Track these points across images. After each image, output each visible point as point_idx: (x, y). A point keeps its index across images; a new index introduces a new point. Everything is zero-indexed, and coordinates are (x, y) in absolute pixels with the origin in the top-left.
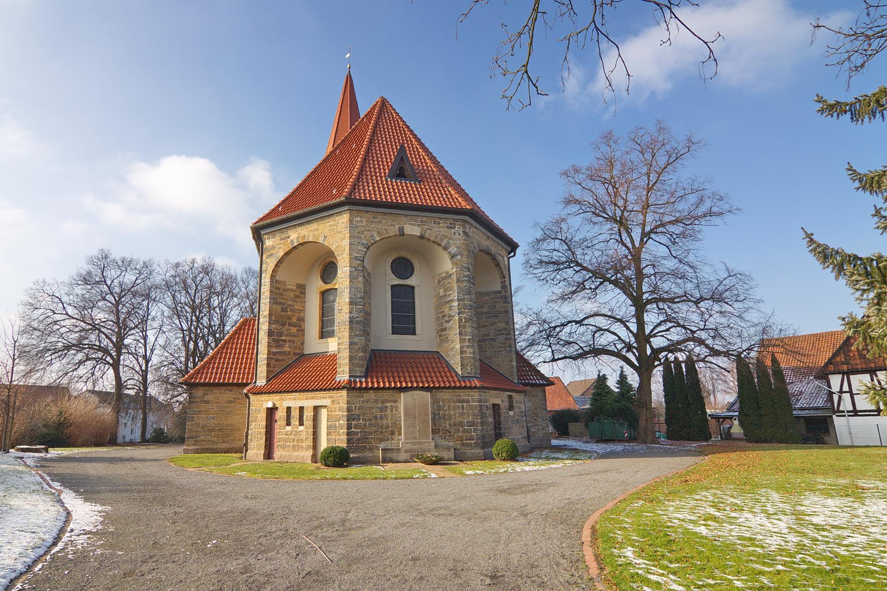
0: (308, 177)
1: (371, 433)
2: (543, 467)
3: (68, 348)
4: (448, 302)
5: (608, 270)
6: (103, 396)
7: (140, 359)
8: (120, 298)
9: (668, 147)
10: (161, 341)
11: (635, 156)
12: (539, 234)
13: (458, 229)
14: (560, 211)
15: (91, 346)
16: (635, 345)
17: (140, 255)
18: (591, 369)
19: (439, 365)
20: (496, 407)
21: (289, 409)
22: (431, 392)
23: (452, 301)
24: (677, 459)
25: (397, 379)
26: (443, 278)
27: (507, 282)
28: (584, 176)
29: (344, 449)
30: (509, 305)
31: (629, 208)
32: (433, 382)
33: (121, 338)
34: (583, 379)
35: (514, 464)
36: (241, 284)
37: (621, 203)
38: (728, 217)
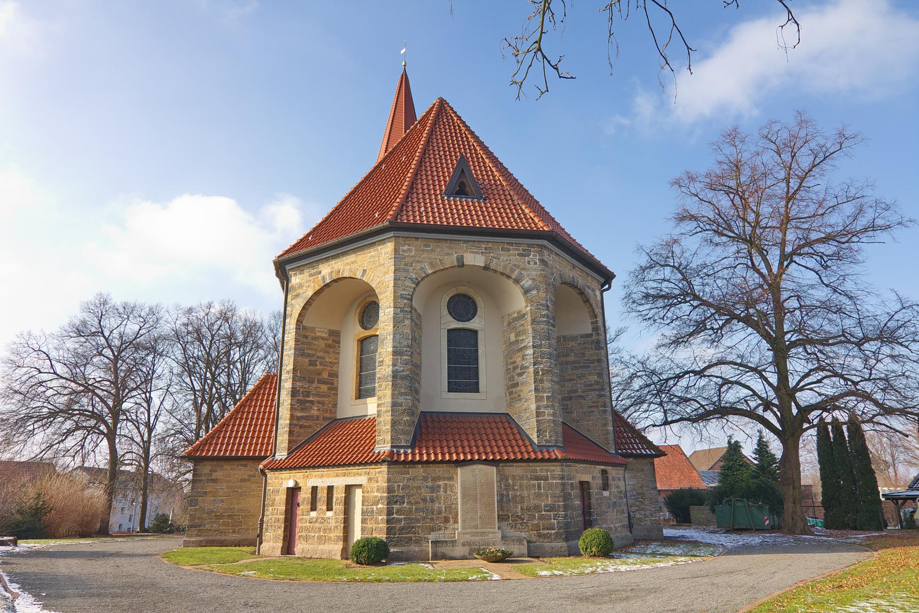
0: (346, 198)
1: (418, 521)
2: (645, 567)
3: (53, 414)
4: (521, 349)
5: (735, 303)
6: (94, 472)
7: (142, 427)
8: (120, 352)
9: (813, 145)
10: (168, 404)
11: (769, 158)
12: (644, 261)
13: (534, 256)
14: (671, 230)
15: (82, 413)
16: (776, 402)
17: (145, 299)
18: (717, 435)
19: (509, 431)
20: (584, 485)
21: (314, 489)
22: (497, 466)
23: (525, 347)
24: (834, 556)
25: (453, 450)
26: (515, 319)
27: (600, 323)
28: (701, 185)
29: (382, 541)
30: (603, 352)
31: (763, 224)
32: (501, 454)
33: (119, 401)
34: (706, 447)
35: (607, 562)
36: (267, 332)
37: (751, 217)
38: (897, 231)
